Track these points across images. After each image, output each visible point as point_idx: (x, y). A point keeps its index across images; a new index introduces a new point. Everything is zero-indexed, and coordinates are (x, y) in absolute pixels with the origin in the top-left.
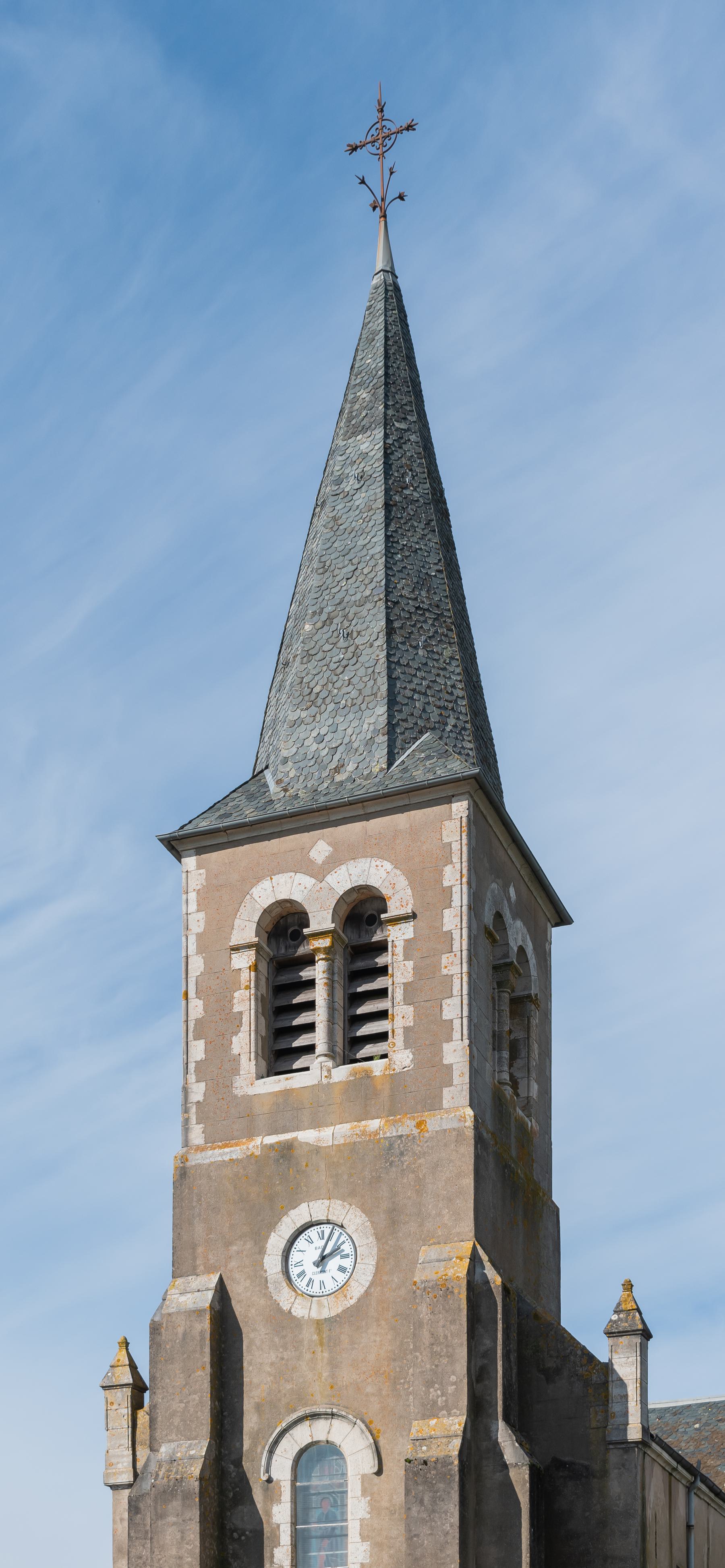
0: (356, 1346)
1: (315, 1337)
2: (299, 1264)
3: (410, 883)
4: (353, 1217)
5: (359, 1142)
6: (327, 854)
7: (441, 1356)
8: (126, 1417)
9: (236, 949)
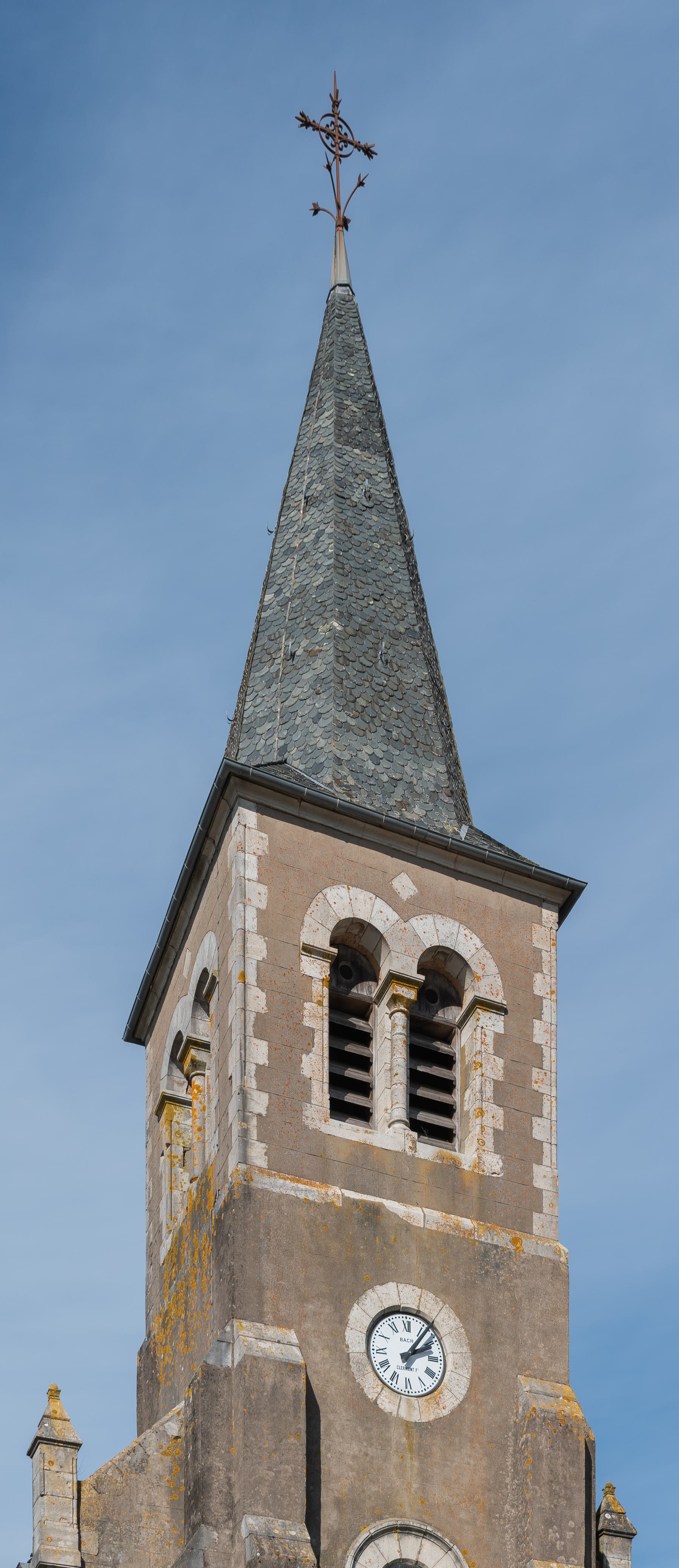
0: (448, 1463)
1: (404, 1440)
2: (381, 1351)
3: (500, 973)
4: (446, 1317)
5: (453, 1236)
6: (412, 893)
7: (560, 1497)
8: (70, 1485)
9: (309, 950)
